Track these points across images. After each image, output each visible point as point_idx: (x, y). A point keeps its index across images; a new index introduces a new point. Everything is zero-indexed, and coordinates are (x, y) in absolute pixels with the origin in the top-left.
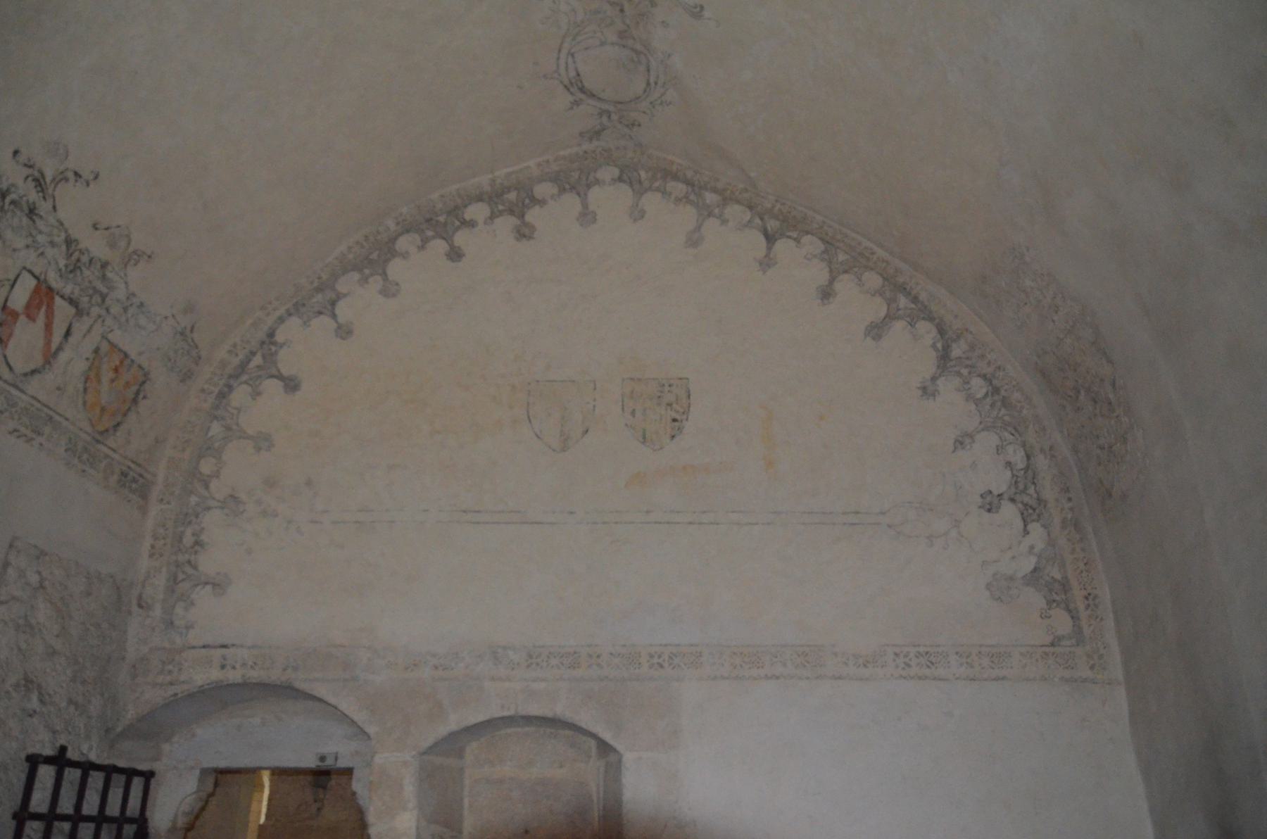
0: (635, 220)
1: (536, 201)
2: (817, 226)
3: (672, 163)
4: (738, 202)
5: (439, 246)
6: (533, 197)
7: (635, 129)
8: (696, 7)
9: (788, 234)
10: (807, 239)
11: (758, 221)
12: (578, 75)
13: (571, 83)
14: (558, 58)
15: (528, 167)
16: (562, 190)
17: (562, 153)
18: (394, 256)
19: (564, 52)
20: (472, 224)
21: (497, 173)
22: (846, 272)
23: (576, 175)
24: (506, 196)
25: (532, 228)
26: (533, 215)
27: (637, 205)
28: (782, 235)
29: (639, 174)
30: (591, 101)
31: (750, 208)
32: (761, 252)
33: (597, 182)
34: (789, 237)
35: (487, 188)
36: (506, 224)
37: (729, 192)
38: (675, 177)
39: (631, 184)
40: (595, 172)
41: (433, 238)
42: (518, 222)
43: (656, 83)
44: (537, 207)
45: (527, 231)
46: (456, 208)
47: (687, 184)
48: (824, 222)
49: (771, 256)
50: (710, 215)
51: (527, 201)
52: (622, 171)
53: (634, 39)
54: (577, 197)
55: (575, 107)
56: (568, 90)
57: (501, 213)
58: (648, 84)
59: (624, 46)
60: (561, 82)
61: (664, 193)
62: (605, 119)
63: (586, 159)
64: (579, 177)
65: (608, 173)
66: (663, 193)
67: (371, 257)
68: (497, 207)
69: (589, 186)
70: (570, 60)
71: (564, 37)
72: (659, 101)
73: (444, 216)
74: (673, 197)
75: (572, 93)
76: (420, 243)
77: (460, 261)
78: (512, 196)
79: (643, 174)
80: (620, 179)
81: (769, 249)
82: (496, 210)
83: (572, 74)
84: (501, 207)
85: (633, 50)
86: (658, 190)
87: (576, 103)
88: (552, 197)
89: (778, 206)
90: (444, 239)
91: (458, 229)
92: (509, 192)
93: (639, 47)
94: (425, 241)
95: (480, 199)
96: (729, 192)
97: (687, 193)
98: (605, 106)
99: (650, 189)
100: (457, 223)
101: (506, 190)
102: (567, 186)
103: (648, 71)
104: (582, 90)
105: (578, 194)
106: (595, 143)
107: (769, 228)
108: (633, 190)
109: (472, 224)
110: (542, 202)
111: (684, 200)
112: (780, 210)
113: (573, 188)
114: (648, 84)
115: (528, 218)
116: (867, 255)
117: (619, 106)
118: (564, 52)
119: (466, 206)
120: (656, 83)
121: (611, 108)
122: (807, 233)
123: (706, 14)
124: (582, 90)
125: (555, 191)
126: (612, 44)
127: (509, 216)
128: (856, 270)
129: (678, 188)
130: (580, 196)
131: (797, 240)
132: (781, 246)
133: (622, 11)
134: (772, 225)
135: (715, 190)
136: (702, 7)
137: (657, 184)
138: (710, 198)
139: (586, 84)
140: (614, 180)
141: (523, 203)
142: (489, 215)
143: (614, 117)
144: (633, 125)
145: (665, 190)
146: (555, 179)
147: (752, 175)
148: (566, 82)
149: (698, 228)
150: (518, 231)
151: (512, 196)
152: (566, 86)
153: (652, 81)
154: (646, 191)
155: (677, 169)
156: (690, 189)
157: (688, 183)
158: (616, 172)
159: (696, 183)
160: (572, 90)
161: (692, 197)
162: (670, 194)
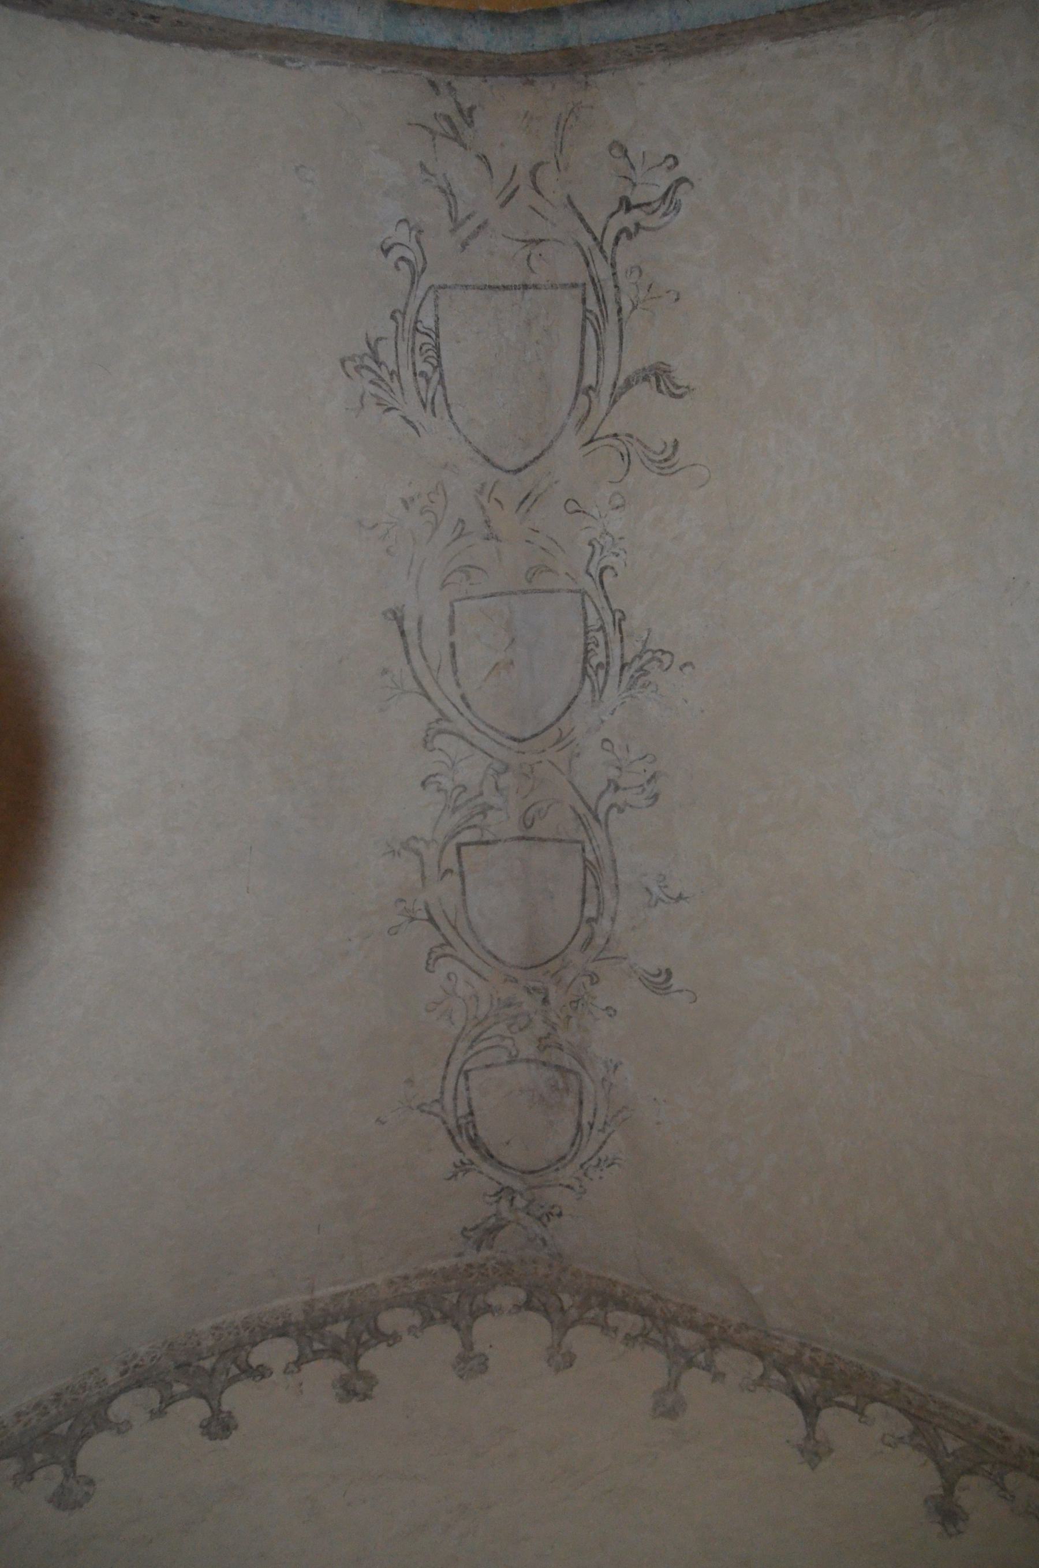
0: (558, 1370)
1: (379, 1336)
2: (887, 1388)
3: (615, 1283)
4: (737, 1345)
5: (196, 1409)
6: (377, 1328)
7: (554, 1222)
8: (659, 975)
9: (840, 1399)
10: (874, 1409)
11: (776, 1376)
12: (471, 1113)
13: (459, 1127)
14: (444, 1078)
15: (373, 1285)
16: (428, 1321)
17: (431, 1266)
18: (99, 1429)
19: (454, 1068)
20: (261, 1372)
21: (318, 1294)
22: (970, 1471)
23: (453, 1297)
24: (328, 1329)
25: (370, 1379)
26: (371, 1360)
27: (559, 1345)
28: (829, 1402)
29: (560, 1299)
30: (486, 1167)
31: (760, 1355)
32: (799, 1431)
33: (488, 1309)
34: (841, 1405)
35: (297, 1316)
36: (330, 1370)
37: (716, 1328)
38: (622, 1305)
39: (546, 1313)
40: (486, 1293)
41: (184, 1396)
42: (346, 1371)
43: (591, 1126)
44: (383, 1346)
45: (360, 1385)
46: (239, 1346)
47: (643, 1316)
48: (897, 1382)
49: (818, 1437)
50: (690, 1363)
51: (365, 1337)
52: (530, 1295)
53: (560, 1048)
54: (454, 1332)
55: (460, 1174)
56: (453, 1139)
57: (317, 1355)
58: (579, 1126)
59: (544, 1064)
60: (444, 1123)
61: (605, 1327)
62: (504, 1204)
63: (471, 1275)
64: (458, 1302)
65: (504, 1297)
66: (603, 1328)
67: (56, 1431)
68: (311, 1347)
69: (474, 1316)
70: (462, 1079)
71: (457, 1039)
72: (594, 1162)
73: (213, 1360)
74: (621, 1335)
75: (459, 1149)
76: (156, 1405)
77: (227, 1437)
78: (341, 1329)
79: (566, 1298)
80: (528, 1305)
81: (811, 1425)
82: (308, 1351)
83: (463, 1110)
84: (317, 1346)
85: (558, 1068)
86: (593, 1322)
87: (463, 1167)
88: (411, 1329)
89: (808, 1354)
90: (204, 1397)
91: (233, 1381)
92: (336, 1321)
93: (567, 1061)
94: (169, 1400)
95: (282, 1332)
96: (716, 1328)
97: (645, 1328)
98: (508, 1181)
99: (579, 1321)
100: (234, 1371)
101: (330, 1319)
102: (438, 1315)
103: (581, 1103)
104: (475, 1142)
105: (456, 1326)
106: (486, 1253)
107: (802, 1390)
108: (551, 1322)
109: (261, 1372)
110: (392, 1339)
111: (640, 1339)
112: (812, 1359)
113: (445, 1317)
114: (579, 1126)
115: (366, 1363)
116: (999, 1441)
117: (532, 1179)
118: (454, 1068)
119: (254, 1344)
120: (591, 1126)
121: (517, 1185)
122: (874, 1400)
123: (676, 983)
124: (475, 1142)
125: (417, 1320)
126: (528, 1061)
127: (331, 1360)
128: (987, 1467)
129: (631, 1322)
130: (459, 1330)
131: (859, 1410)
132: (829, 1419)
133: (545, 1001)
134: (805, 1384)
135: (692, 1326)
136: (669, 973)
137: (591, 1314)
138: (686, 1337)
139: (481, 1133)
140: (518, 1308)
141: (358, 1340)
142: (294, 1357)
143: (520, 1202)
144: (549, 1215)
145: (606, 1323)
146: (417, 1302)
147: (756, 1291)
148: (452, 1122)
149: (674, 1384)
150: (344, 1387)
151: (341, 1329)
152: (449, 1132)
153: (585, 1122)
154: (574, 1324)
155: (624, 1292)
156: (649, 1324)
157: (643, 1312)
158: (522, 1296)
159: (658, 1312)
160: (458, 1139)
161: (654, 1335)
162: (616, 1330)
